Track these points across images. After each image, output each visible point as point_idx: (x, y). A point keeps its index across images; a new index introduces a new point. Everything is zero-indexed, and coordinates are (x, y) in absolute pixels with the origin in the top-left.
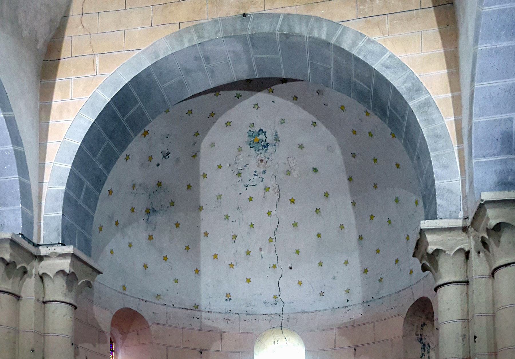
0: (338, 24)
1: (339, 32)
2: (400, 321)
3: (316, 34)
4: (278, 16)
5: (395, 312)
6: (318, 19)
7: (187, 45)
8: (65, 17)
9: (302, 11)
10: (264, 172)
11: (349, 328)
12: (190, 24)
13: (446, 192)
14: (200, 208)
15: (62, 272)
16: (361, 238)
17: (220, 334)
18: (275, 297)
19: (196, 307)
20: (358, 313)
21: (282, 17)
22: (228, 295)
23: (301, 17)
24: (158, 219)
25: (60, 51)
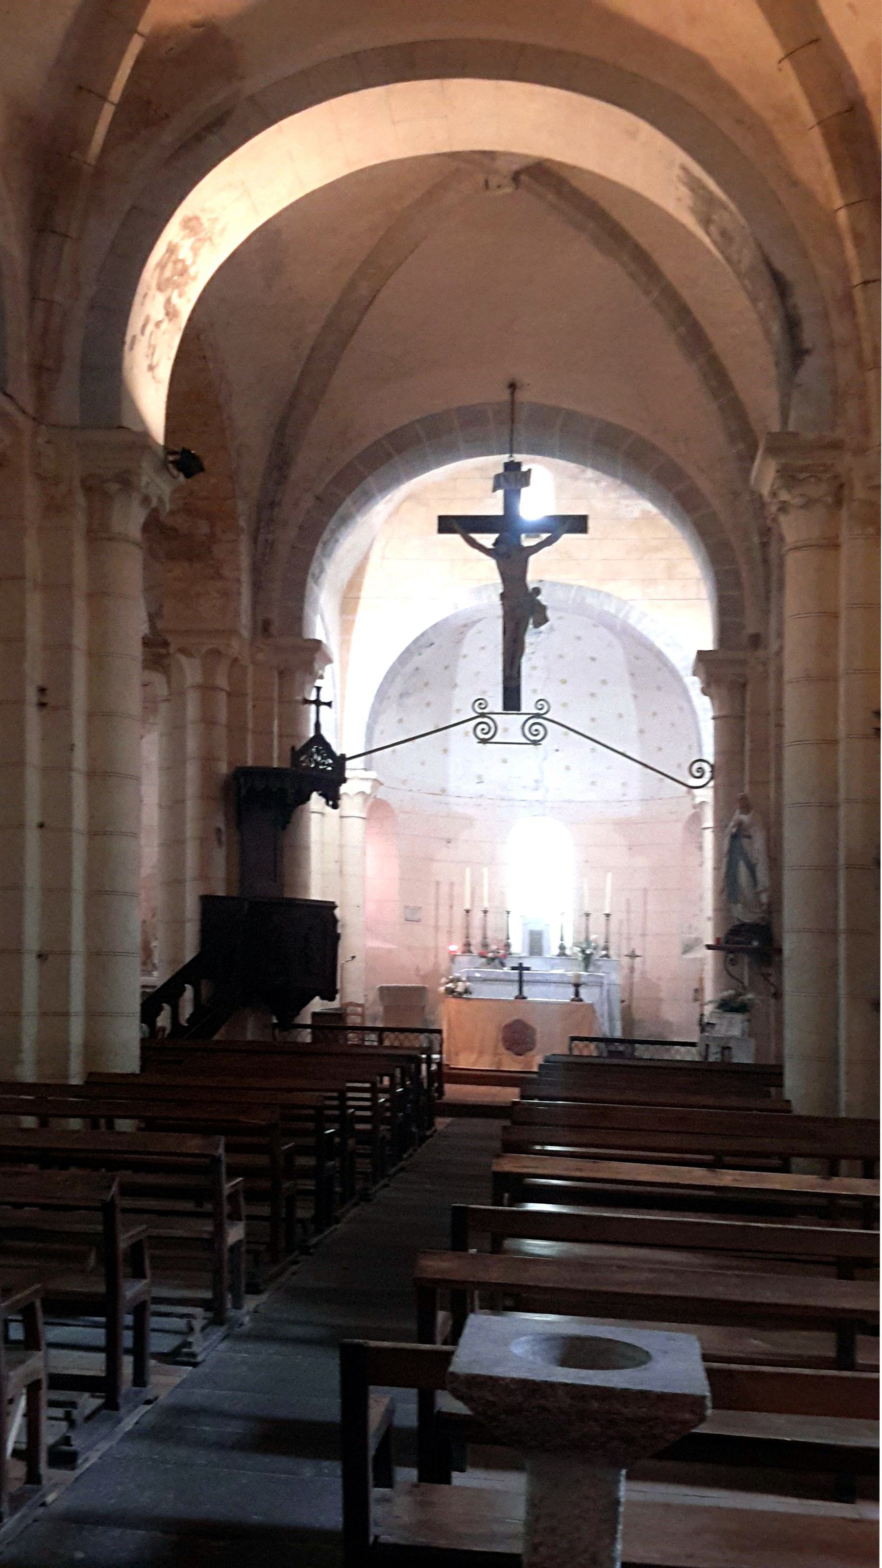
0: (625, 602)
1: (627, 607)
2: (680, 826)
3: (606, 608)
4: (571, 586)
5: (674, 816)
6: (608, 595)
7: (485, 601)
8: (366, 558)
9: (593, 585)
10: (533, 653)
11: (623, 825)
12: (490, 582)
13: (828, 475)
14: (455, 686)
15: (363, 793)
16: (641, 731)
17: (469, 821)
18: (536, 781)
19: (444, 791)
20: (635, 810)
21: (575, 588)
22: (479, 777)
23: (593, 591)
24: (409, 701)
25: (360, 590)
